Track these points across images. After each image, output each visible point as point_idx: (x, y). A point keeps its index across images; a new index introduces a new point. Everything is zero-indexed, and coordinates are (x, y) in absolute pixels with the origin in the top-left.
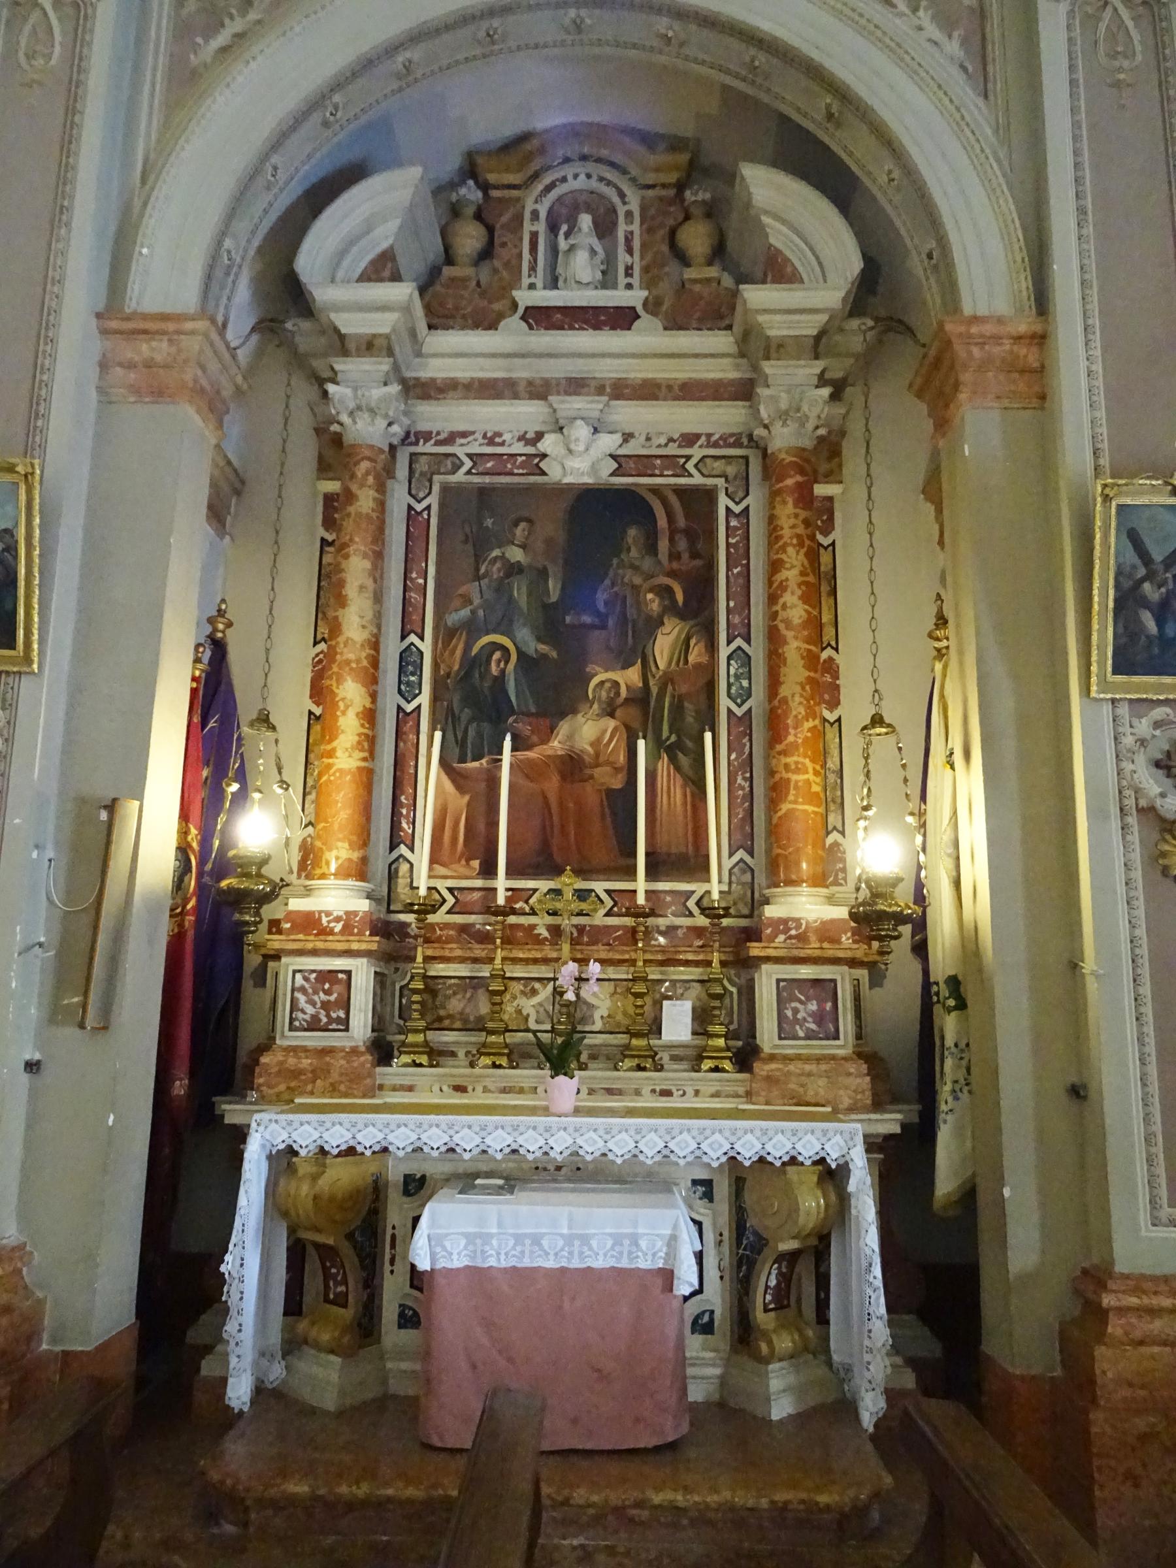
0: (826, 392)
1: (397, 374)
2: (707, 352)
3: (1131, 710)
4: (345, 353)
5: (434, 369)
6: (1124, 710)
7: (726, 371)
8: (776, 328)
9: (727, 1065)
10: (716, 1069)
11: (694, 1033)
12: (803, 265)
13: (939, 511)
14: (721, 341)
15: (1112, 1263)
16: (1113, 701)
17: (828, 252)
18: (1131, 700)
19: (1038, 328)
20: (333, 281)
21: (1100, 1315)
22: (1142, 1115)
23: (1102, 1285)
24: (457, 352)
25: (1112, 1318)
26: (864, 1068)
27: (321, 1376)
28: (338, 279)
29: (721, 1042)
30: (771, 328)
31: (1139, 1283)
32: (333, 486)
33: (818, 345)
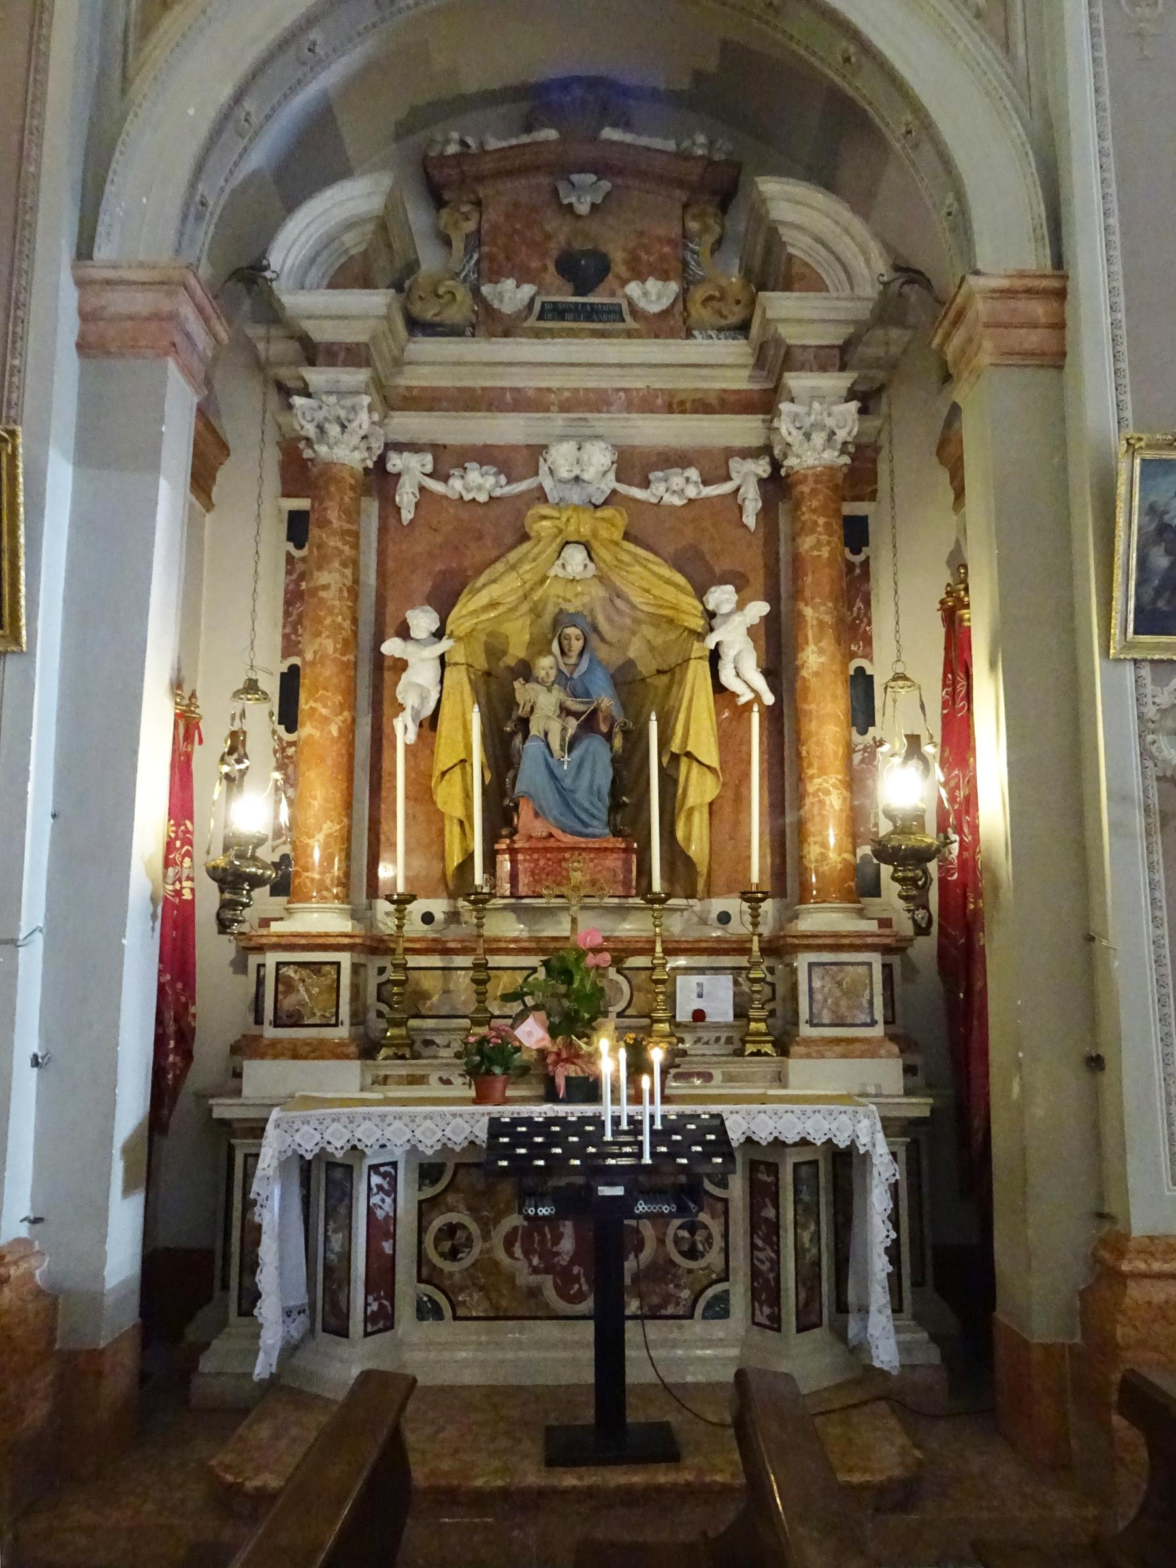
0: (854, 406)
1: (379, 386)
2: (723, 361)
3: (1153, 672)
4: (312, 362)
5: (414, 379)
6: (1146, 672)
7: (740, 381)
8: (792, 335)
9: (768, 1048)
10: (758, 1053)
11: (735, 1016)
12: (828, 274)
13: (417, 363)
14: (734, 350)
15: (1130, 1233)
16: (1135, 661)
17: (858, 265)
18: (1152, 661)
19: (1055, 284)
20: (303, 288)
21: (1118, 1278)
22: (1153, 957)
23: (1121, 1254)
24: (435, 361)
25: (1131, 1284)
26: (895, 1049)
27: (446, 1270)
28: (307, 283)
29: (762, 1027)
30: (790, 337)
31: (1154, 1246)
32: (302, 504)
33: (840, 356)
